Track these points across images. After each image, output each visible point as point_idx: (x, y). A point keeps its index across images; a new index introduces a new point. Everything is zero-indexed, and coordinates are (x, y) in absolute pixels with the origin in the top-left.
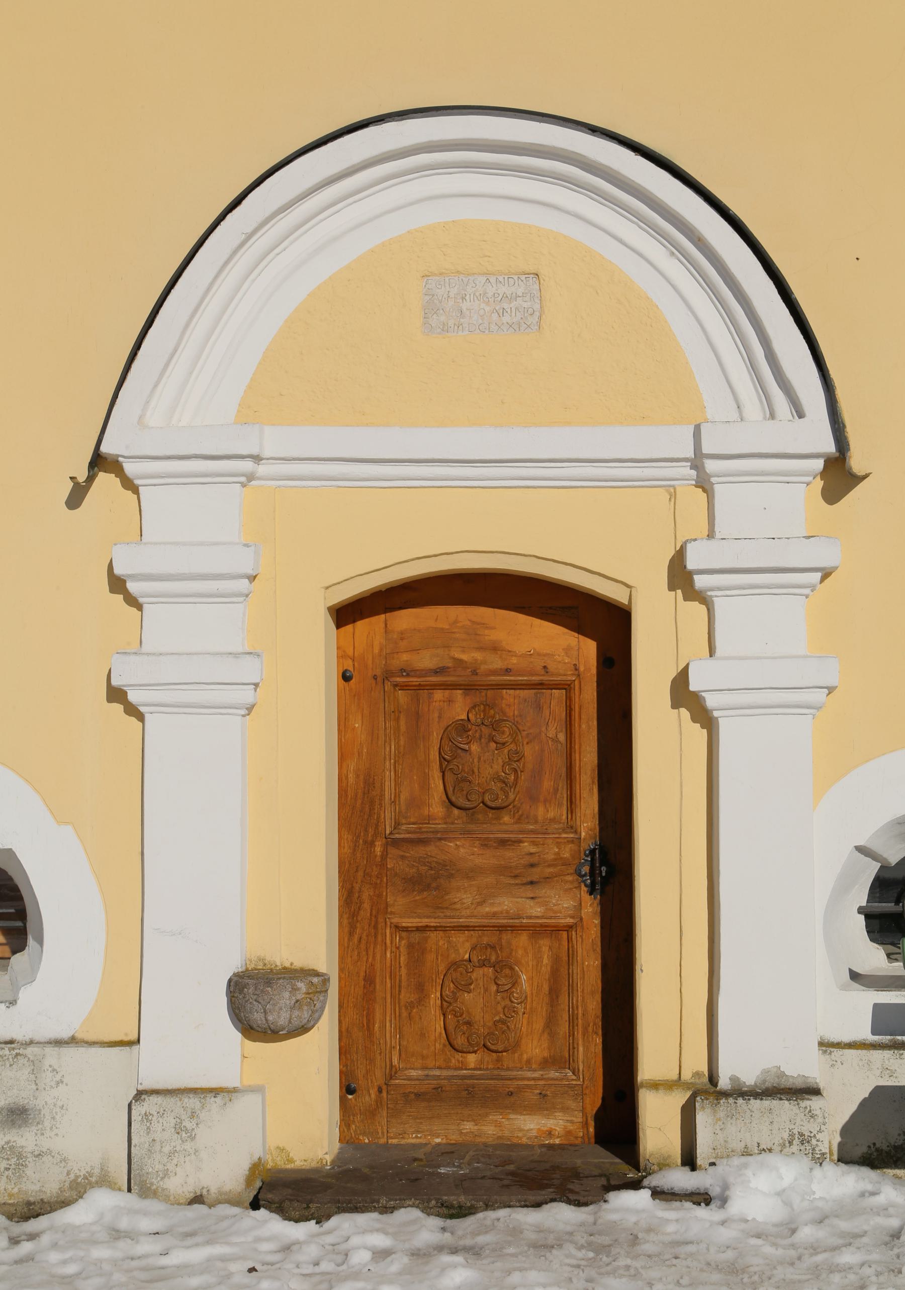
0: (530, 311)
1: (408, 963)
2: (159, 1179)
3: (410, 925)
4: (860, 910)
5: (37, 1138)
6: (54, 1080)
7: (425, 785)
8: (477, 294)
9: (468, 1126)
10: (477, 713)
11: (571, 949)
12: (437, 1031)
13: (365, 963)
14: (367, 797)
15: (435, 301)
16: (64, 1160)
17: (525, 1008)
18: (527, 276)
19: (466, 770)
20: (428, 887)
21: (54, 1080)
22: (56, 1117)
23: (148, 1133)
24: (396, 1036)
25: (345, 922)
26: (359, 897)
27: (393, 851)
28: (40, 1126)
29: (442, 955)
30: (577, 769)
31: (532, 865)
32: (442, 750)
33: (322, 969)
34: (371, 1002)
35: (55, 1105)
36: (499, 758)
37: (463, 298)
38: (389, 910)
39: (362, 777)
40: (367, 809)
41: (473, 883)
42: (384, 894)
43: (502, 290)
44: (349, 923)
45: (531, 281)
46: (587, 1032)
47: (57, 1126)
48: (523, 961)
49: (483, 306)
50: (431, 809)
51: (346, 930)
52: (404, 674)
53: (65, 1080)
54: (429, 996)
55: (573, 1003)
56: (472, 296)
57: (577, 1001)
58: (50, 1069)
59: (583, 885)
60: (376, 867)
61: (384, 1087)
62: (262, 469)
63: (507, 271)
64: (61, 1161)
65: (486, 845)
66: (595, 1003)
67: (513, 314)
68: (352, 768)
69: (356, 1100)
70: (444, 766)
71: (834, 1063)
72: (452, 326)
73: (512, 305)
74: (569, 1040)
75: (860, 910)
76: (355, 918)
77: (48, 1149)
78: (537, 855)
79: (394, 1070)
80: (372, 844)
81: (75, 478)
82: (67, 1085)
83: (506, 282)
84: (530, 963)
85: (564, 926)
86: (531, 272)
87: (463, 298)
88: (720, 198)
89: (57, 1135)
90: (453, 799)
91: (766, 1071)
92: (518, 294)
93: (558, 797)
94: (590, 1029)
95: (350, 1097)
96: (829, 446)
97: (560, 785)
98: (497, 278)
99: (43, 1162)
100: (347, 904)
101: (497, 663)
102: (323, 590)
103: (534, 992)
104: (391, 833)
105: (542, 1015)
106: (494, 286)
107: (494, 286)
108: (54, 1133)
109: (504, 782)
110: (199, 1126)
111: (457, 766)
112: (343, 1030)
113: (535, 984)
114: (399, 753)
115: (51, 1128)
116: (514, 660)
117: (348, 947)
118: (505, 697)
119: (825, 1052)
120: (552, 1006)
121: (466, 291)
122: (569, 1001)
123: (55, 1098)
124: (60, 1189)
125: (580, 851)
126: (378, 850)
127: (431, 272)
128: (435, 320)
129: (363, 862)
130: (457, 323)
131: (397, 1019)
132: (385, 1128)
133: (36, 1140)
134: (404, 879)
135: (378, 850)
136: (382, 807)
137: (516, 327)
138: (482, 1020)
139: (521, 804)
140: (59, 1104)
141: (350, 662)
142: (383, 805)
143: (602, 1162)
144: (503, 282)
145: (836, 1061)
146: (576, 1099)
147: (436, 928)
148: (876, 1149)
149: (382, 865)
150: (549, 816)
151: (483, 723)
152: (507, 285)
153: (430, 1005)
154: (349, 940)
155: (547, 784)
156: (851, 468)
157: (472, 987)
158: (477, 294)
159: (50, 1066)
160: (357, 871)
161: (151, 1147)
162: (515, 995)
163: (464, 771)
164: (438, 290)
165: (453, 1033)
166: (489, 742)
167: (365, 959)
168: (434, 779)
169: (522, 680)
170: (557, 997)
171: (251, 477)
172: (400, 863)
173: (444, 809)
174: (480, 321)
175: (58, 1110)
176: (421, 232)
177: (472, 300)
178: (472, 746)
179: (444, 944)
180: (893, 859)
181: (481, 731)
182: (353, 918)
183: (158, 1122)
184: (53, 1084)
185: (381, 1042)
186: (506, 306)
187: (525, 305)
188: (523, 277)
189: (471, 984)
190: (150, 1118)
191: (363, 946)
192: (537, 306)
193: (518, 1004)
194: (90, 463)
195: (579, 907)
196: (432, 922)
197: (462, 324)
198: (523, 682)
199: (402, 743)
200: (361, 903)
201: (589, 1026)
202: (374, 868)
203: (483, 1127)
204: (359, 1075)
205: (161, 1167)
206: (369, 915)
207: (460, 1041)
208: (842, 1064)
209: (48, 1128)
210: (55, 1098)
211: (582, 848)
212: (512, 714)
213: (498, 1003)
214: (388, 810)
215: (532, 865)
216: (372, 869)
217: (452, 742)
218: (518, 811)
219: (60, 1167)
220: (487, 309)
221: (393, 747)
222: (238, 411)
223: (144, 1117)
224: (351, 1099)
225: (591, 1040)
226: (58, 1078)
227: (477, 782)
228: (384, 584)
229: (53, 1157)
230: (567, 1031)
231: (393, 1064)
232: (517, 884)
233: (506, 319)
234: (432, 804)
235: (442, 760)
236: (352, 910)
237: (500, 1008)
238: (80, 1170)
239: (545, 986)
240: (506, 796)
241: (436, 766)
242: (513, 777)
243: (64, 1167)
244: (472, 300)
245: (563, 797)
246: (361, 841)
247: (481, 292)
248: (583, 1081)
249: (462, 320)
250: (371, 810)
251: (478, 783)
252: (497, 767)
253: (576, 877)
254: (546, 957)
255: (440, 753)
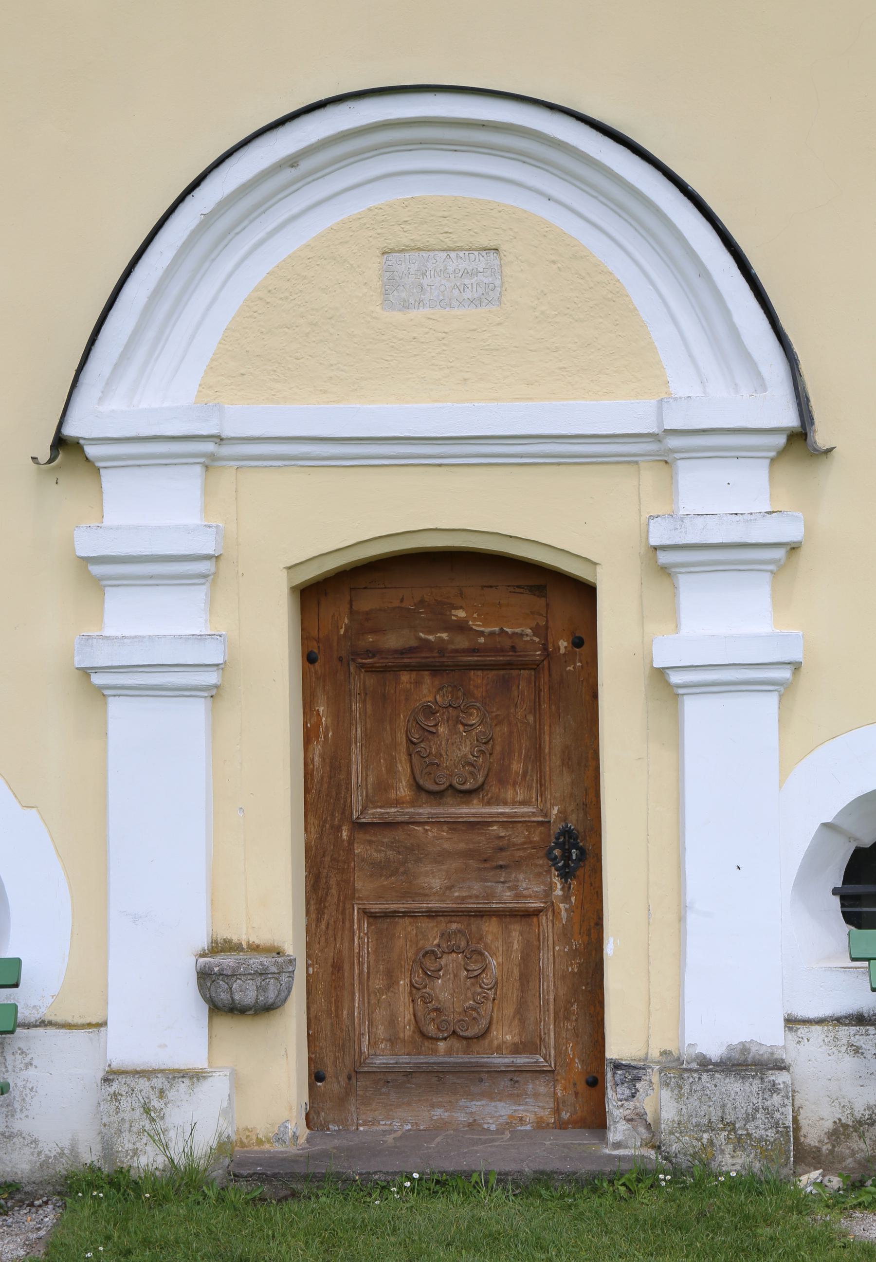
0: (491, 286)
1: (376, 949)
2: (129, 1157)
3: (377, 910)
4: (835, 891)
5: (7, 1119)
6: (24, 1062)
7: (392, 769)
8: (438, 270)
9: (438, 1113)
10: (444, 695)
11: (541, 934)
12: (406, 1018)
13: (333, 949)
14: (334, 781)
15: (396, 277)
16: (35, 1142)
17: (495, 994)
18: (487, 252)
19: (434, 753)
20: (395, 873)
21: (24, 1062)
22: (26, 1099)
23: (117, 1113)
24: (365, 1022)
25: (312, 908)
26: (326, 882)
27: (360, 836)
28: (10, 1108)
29: (411, 941)
30: (547, 751)
31: (501, 849)
32: (408, 732)
33: (289, 949)
34: (339, 989)
35: (24, 1087)
36: (467, 740)
37: (424, 274)
38: (357, 895)
39: (328, 761)
40: (334, 794)
41: (443, 867)
42: (352, 879)
43: (463, 265)
44: (317, 909)
45: (492, 257)
46: (559, 1017)
47: (27, 1107)
48: (493, 946)
49: (443, 282)
50: (398, 793)
51: (314, 916)
52: (370, 655)
53: (34, 1063)
54: (398, 983)
55: (543, 989)
56: (432, 272)
57: (548, 986)
58: (19, 1052)
59: (553, 869)
60: (344, 852)
61: (353, 1074)
62: (226, 450)
63: (468, 247)
64: (31, 1143)
65: (454, 829)
66: (566, 989)
67: (475, 290)
68: (318, 752)
69: (325, 1087)
70: (411, 749)
71: (800, 1039)
72: (413, 302)
73: (474, 280)
74: (540, 1025)
75: (835, 891)
76: (322, 904)
77: (18, 1131)
78: (506, 838)
79: (363, 1057)
80: (339, 829)
81: (37, 458)
82: (36, 1067)
83: (467, 258)
84: (501, 949)
85: (534, 911)
86: (492, 248)
87: (424, 274)
88: (679, 175)
89: (27, 1116)
90: (421, 782)
91: (731, 1048)
92: (479, 269)
93: (527, 779)
94: (561, 1015)
95: (319, 1084)
96: (790, 419)
97: (530, 768)
98: (457, 254)
99: (14, 1143)
100: (314, 890)
101: (462, 642)
102: (285, 571)
103: (505, 978)
104: (358, 818)
105: (513, 1001)
106: (455, 262)
107: (455, 262)
108: (24, 1115)
109: (473, 765)
110: (168, 1105)
111: (424, 748)
112: (312, 1015)
113: (505, 969)
114: (366, 735)
115: (21, 1110)
116: (482, 640)
117: (316, 934)
118: (472, 677)
119: (790, 1029)
120: (522, 992)
121: (426, 267)
122: (540, 987)
123: (24, 1080)
124: (31, 1170)
125: (549, 835)
126: (345, 834)
127: (391, 249)
128: (396, 297)
129: (330, 847)
130: (418, 300)
131: (366, 1005)
132: (355, 1116)
133: (7, 1121)
134: (372, 864)
135: (345, 834)
136: (348, 790)
137: (477, 303)
138: (451, 1006)
139: (490, 787)
140: (29, 1085)
141: (315, 644)
142: (350, 789)
143: (571, 1143)
144: (463, 257)
145: (802, 1038)
146: (547, 1085)
147: (406, 914)
148: (842, 1124)
149: (350, 849)
150: (518, 799)
151: (450, 705)
152: (467, 261)
153: (399, 991)
154: (316, 926)
155: (517, 767)
156: (815, 442)
157: (441, 973)
158: (438, 270)
159: (19, 1049)
160: (324, 856)
161: (121, 1126)
162: (485, 980)
163: (432, 753)
164: (398, 267)
165: (423, 1019)
166: (457, 724)
167: (333, 945)
168: (401, 762)
169: (490, 661)
170: (528, 982)
171: (213, 457)
172: (368, 847)
173: (412, 793)
174: (441, 298)
175: (28, 1092)
176: (381, 208)
177: (433, 276)
178: (439, 728)
179: (413, 929)
180: (867, 842)
181: (448, 712)
182: (320, 904)
183: (127, 1102)
184: (22, 1066)
185: (350, 1028)
186: (467, 281)
187: (486, 280)
188: (484, 253)
189: (440, 970)
190: (119, 1097)
191: (330, 932)
192: (498, 282)
193: (488, 990)
194: (51, 446)
195: (551, 887)
196: (401, 907)
197: (422, 300)
198: (492, 663)
199: (369, 726)
200: (329, 888)
201: (560, 1011)
202: (341, 852)
203: (453, 1114)
204: (328, 1062)
205: (131, 1146)
206: (336, 900)
207: (431, 1029)
208: (808, 1041)
209: (18, 1110)
210: (24, 1080)
211: (552, 831)
212: (479, 695)
213: (468, 989)
214: (354, 794)
215: (501, 849)
216: (339, 855)
217: (419, 724)
218: (487, 795)
219: (31, 1148)
220: (448, 284)
221: (359, 730)
222: (199, 391)
223: (113, 1097)
224: (320, 1087)
225: (562, 1025)
226: (27, 1060)
227: (445, 765)
228: (347, 564)
229: (24, 1138)
230: (538, 1017)
231: (363, 1051)
232: (485, 869)
233: (468, 295)
234: (399, 788)
235: (409, 743)
236: (320, 895)
237: (469, 994)
238: (50, 1151)
239: (515, 971)
240: (474, 779)
241: (403, 748)
242: (481, 760)
243: (35, 1148)
244: (433, 276)
245: (533, 780)
246: (328, 826)
247: (442, 268)
248: (555, 1067)
249: (422, 296)
250: (338, 793)
251: (446, 766)
252: (466, 749)
253: (546, 861)
254: (516, 942)
255: (407, 737)
